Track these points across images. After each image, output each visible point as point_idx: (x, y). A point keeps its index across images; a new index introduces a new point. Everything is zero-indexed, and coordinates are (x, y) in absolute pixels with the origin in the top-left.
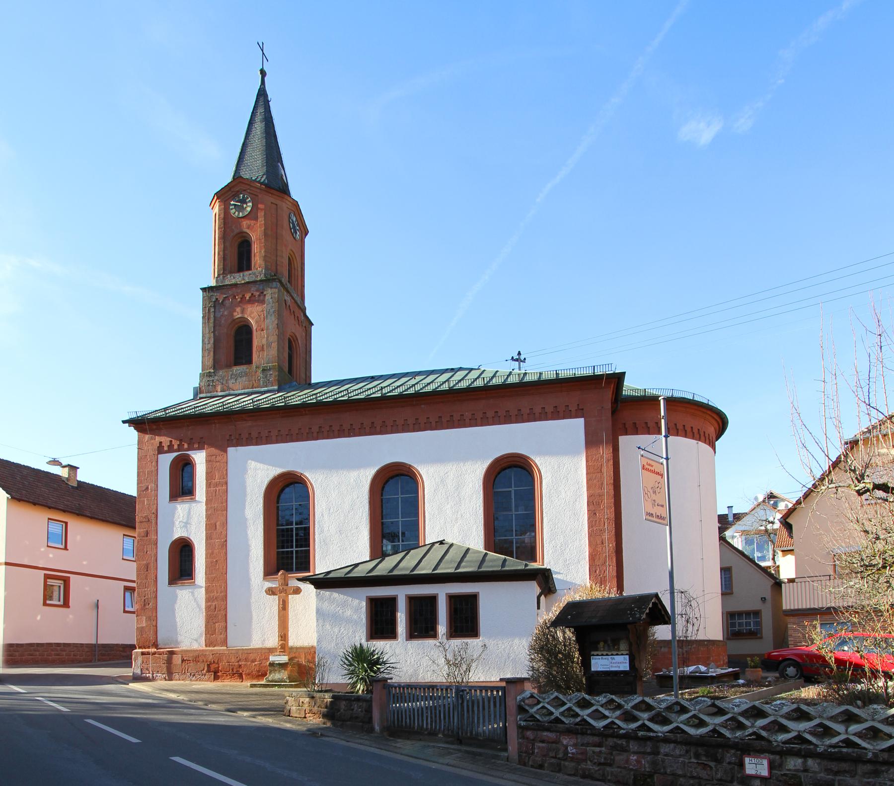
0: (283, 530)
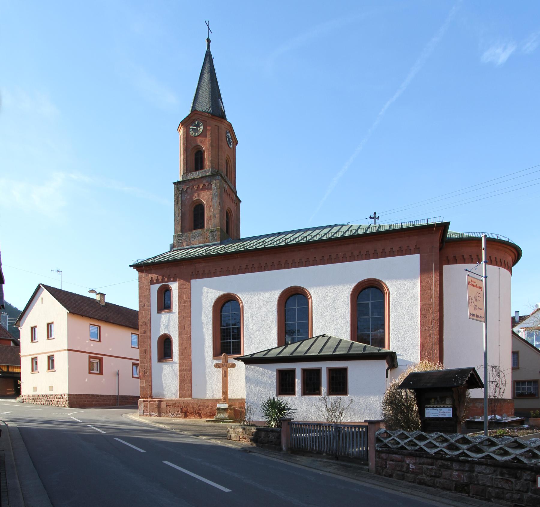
0: (224, 329)
